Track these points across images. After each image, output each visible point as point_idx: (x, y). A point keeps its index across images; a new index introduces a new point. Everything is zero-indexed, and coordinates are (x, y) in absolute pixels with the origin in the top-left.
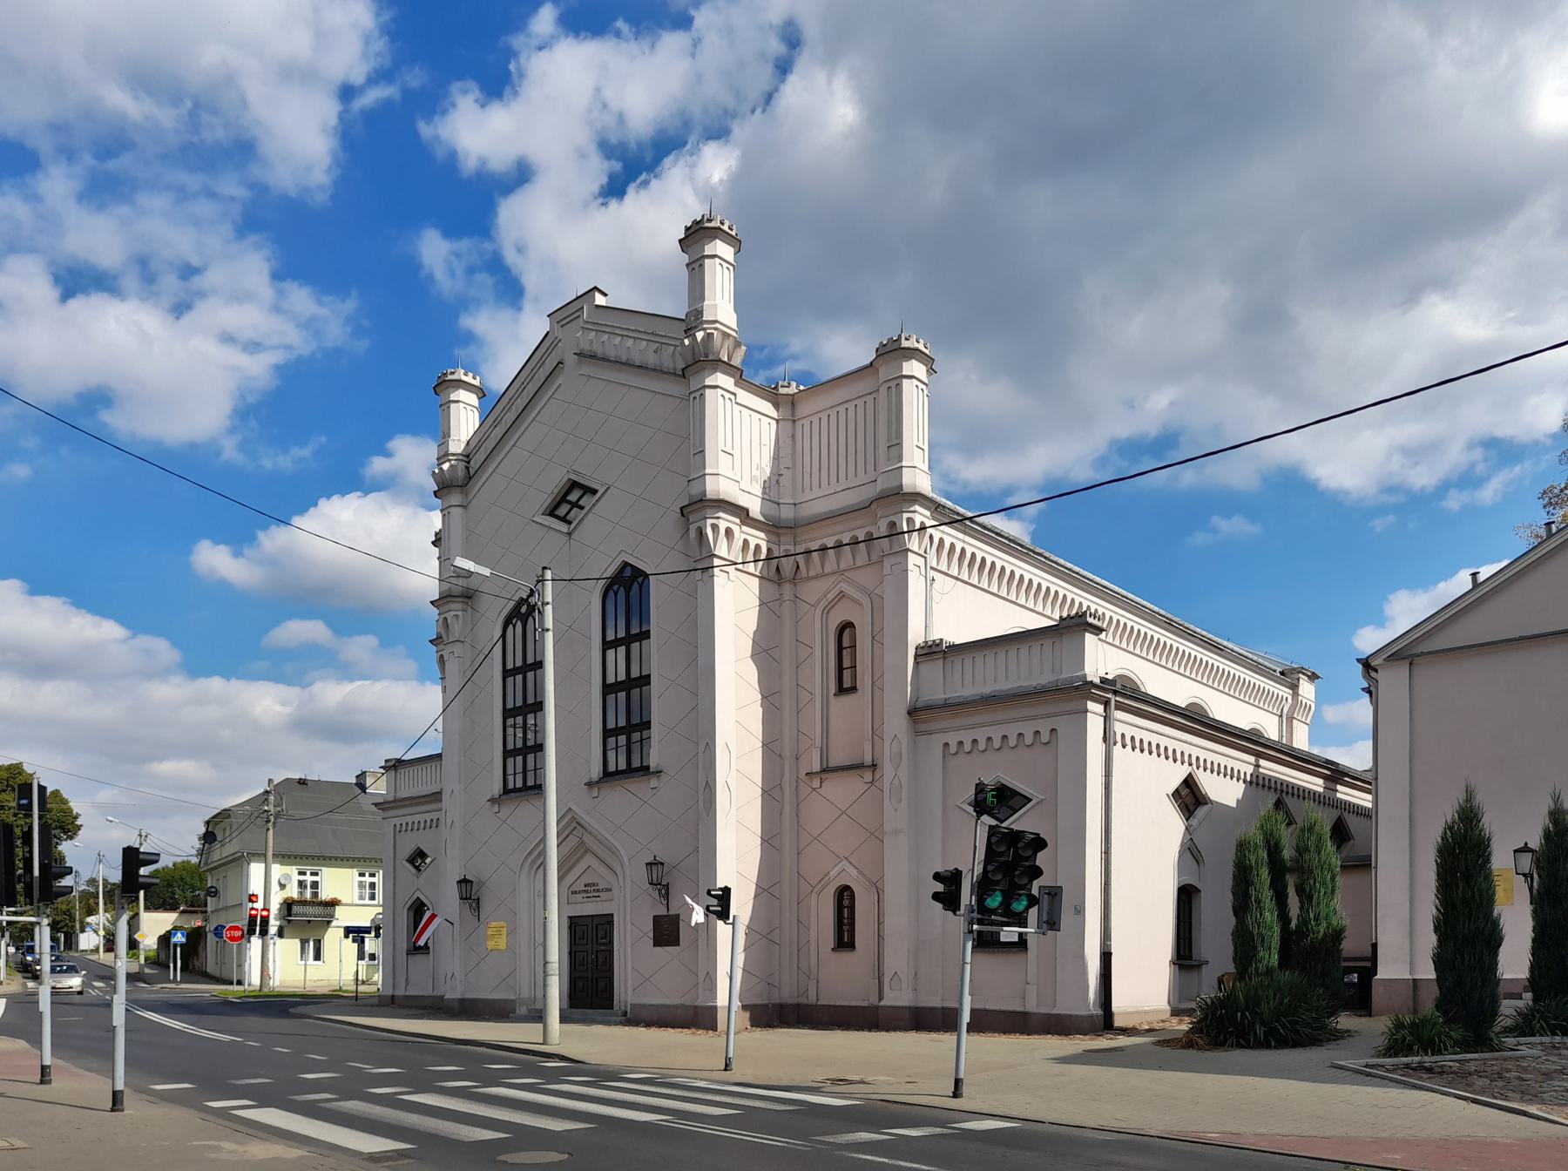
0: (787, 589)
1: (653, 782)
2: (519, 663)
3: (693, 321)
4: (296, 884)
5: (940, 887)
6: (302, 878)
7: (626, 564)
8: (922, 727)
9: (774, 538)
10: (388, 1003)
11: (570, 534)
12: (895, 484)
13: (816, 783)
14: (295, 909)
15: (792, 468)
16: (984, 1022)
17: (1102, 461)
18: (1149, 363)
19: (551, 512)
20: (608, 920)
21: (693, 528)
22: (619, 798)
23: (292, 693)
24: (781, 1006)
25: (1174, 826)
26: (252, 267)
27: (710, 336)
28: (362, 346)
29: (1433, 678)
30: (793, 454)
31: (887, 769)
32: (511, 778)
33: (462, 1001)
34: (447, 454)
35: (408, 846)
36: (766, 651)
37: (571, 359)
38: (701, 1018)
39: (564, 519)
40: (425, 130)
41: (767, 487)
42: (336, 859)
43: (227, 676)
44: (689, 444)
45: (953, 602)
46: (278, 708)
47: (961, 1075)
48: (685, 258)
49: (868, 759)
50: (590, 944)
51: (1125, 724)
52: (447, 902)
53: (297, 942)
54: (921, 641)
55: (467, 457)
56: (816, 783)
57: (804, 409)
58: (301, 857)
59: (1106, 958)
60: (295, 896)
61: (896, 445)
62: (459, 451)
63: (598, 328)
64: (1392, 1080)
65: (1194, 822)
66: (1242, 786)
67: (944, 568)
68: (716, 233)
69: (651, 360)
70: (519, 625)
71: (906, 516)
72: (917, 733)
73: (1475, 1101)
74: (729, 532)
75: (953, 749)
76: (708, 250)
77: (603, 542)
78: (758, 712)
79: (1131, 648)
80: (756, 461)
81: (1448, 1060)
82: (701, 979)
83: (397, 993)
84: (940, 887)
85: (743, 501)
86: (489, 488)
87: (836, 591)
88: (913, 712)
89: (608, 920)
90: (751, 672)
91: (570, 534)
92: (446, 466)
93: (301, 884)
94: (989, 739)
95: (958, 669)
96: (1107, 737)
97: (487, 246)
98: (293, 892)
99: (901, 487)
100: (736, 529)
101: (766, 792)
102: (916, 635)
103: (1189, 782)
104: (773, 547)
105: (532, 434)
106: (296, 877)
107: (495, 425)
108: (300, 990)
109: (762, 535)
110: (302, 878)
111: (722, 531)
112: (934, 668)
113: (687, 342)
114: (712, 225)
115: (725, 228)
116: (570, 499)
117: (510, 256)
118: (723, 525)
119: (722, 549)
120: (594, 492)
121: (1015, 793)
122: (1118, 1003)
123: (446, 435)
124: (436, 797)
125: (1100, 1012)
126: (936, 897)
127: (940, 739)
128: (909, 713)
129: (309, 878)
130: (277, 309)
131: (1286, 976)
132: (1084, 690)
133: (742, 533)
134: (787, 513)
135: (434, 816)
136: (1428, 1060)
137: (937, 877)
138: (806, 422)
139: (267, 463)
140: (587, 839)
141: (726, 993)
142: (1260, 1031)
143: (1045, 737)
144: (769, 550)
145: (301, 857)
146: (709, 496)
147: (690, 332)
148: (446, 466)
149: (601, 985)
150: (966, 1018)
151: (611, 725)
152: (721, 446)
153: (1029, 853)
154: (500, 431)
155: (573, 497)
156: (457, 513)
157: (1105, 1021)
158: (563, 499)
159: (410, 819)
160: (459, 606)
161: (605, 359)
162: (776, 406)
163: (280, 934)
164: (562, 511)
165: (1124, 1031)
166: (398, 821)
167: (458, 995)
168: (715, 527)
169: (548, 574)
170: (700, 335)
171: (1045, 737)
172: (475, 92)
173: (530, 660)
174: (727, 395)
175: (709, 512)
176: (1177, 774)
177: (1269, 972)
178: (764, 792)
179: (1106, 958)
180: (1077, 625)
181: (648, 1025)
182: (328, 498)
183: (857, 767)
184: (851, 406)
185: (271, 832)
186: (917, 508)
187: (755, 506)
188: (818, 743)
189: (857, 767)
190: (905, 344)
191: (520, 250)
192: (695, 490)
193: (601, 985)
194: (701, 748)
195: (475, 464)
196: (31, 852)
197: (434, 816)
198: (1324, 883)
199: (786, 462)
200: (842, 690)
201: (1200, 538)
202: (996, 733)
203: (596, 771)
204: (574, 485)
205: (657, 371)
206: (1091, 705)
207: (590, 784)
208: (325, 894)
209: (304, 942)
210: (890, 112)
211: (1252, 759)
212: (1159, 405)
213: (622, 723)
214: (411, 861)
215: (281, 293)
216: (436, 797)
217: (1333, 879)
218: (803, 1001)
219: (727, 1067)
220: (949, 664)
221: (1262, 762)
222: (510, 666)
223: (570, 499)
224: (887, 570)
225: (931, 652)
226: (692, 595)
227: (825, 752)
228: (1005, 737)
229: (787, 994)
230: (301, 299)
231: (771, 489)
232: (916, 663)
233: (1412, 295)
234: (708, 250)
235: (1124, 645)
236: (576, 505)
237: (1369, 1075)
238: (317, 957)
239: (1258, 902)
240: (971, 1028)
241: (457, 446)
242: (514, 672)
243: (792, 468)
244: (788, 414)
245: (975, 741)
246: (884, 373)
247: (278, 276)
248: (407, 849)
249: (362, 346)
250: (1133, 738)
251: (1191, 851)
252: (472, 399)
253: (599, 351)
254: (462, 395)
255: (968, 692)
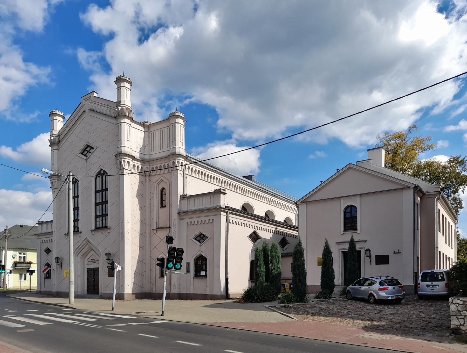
0: (147, 178)
1: (108, 231)
2: (101, 189)
3: (118, 104)
4: (18, 257)
5: (159, 262)
6: (20, 255)
7: (102, 169)
8: (182, 217)
9: (143, 164)
10: (39, 293)
11: (87, 160)
12: (174, 151)
13: (155, 232)
14: (18, 265)
15: (149, 145)
16: (169, 297)
17: (283, 134)
18: (296, 108)
19: (82, 153)
20: (97, 269)
21: (118, 161)
22: (100, 235)
23: (30, 194)
24: (145, 293)
25: (250, 245)
26: (16, 57)
27: (122, 108)
28: (54, 84)
29: (311, 207)
30: (149, 141)
31: (173, 229)
32: (98, 223)
33: (57, 292)
34: (53, 135)
35: (45, 247)
36: (141, 195)
37: (87, 111)
38: (120, 297)
39: (86, 156)
40: (82, 16)
41: (141, 150)
42: (31, 249)
43: (8, 189)
44: (117, 137)
45: (191, 184)
46: (27, 200)
47: (163, 310)
48: (116, 86)
49: (168, 226)
50: (93, 275)
51: (232, 217)
52: (54, 265)
53: (18, 275)
54: (182, 194)
55: (59, 136)
56: (155, 232)
57: (152, 129)
58: (20, 249)
59: (227, 280)
60: (18, 261)
61: (174, 141)
62: (57, 134)
63: (94, 102)
64: (273, 310)
65: (256, 243)
66: (272, 234)
67: (190, 174)
68: (125, 80)
69: (108, 113)
70: (101, 177)
71: (177, 160)
72: (181, 219)
73: (283, 314)
74: (128, 162)
75: (189, 223)
76: (122, 85)
77: (97, 161)
78: (139, 212)
79: (249, 196)
80: (138, 142)
81: (291, 305)
82: (121, 285)
83: (41, 290)
84: (159, 262)
85: (133, 154)
86: (65, 145)
87: (160, 179)
88: (179, 213)
89: (97, 269)
90: (136, 201)
91: (87, 160)
92: (52, 138)
93: (20, 257)
94: (202, 221)
95: (191, 203)
96: (228, 221)
97: (100, 54)
98: (17, 259)
99: (176, 152)
100: (131, 162)
101: (141, 234)
102: (180, 192)
103: (255, 233)
104: (143, 166)
105: (77, 130)
106: (18, 255)
107: (67, 127)
108: (19, 289)
109: (140, 163)
110: (20, 255)
111: (126, 162)
112: (185, 201)
113: (116, 109)
114: (123, 78)
115: (127, 79)
116: (87, 150)
117: (108, 58)
118: (126, 161)
119: (126, 166)
120: (93, 148)
121: (204, 236)
122: (230, 292)
123: (53, 129)
124: (51, 233)
125: (225, 294)
126: (158, 265)
127: (185, 221)
128: (178, 214)
129: (22, 255)
130: (27, 71)
131: (265, 284)
132: (219, 209)
133: (132, 163)
134: (147, 157)
135: (50, 238)
136: (287, 305)
137: (158, 260)
138: (152, 133)
139: (22, 120)
140: (91, 246)
141: (128, 289)
142: (256, 298)
143: (211, 221)
144: (142, 167)
145: (20, 249)
146: (122, 152)
147: (117, 107)
148: (52, 138)
149: (96, 288)
150: (165, 295)
151: (98, 214)
152: (126, 139)
153: (180, 253)
154: (68, 129)
155: (88, 149)
156: (55, 151)
157: (227, 296)
158: (85, 150)
159: (45, 239)
160: (56, 178)
161: (96, 112)
162: (144, 128)
163: (10, 272)
164: (85, 153)
165: (231, 299)
166: (42, 240)
167: (55, 291)
168: (124, 161)
169: (71, 174)
170: (120, 108)
171: (211, 221)
172: (96, 7)
173: (104, 188)
174: (128, 125)
175: (122, 157)
176: (251, 231)
177: (262, 283)
178: (140, 234)
179: (227, 280)
180: (218, 192)
181: (106, 299)
182: (43, 133)
183: (166, 228)
184: (164, 129)
185: (7, 242)
186: (180, 158)
187: (137, 155)
188: (156, 221)
189: (166, 228)
190: (176, 114)
191: (112, 57)
192: (119, 150)
193: (96, 288)
194: (121, 221)
195: (61, 138)
196: (74, 214)
197: (50, 238)
198: (276, 261)
199: (147, 143)
200: (163, 206)
201: (311, 157)
202: (200, 219)
203: (93, 227)
204: (88, 146)
205: (110, 116)
206: (222, 213)
207: (92, 231)
208: (28, 260)
209: (21, 275)
210: (227, 26)
211: (275, 227)
212: (298, 118)
213: (101, 214)
214: (46, 251)
215: (26, 65)
216: (51, 233)
217: (279, 260)
218: (151, 292)
219: (113, 310)
220: (189, 201)
221: (278, 227)
222: (98, 189)
223: (87, 150)
224: (172, 175)
225: (184, 197)
226: (119, 179)
227: (157, 223)
228: (202, 221)
229: (147, 290)
230: (34, 68)
231: (142, 151)
232: (180, 200)
233: (371, 91)
234: (122, 85)
235: (249, 196)
236: (89, 152)
237: (269, 308)
238: (25, 279)
239: (260, 265)
240: (166, 298)
241: (56, 132)
242: (99, 191)
243: (149, 145)
244: (147, 130)
245: (195, 222)
246: (172, 121)
247: (25, 60)
248: (44, 248)
249: (54, 84)
250: (238, 222)
251: (256, 251)
252: (61, 119)
253: (95, 109)
254: (57, 118)
255: (193, 208)
